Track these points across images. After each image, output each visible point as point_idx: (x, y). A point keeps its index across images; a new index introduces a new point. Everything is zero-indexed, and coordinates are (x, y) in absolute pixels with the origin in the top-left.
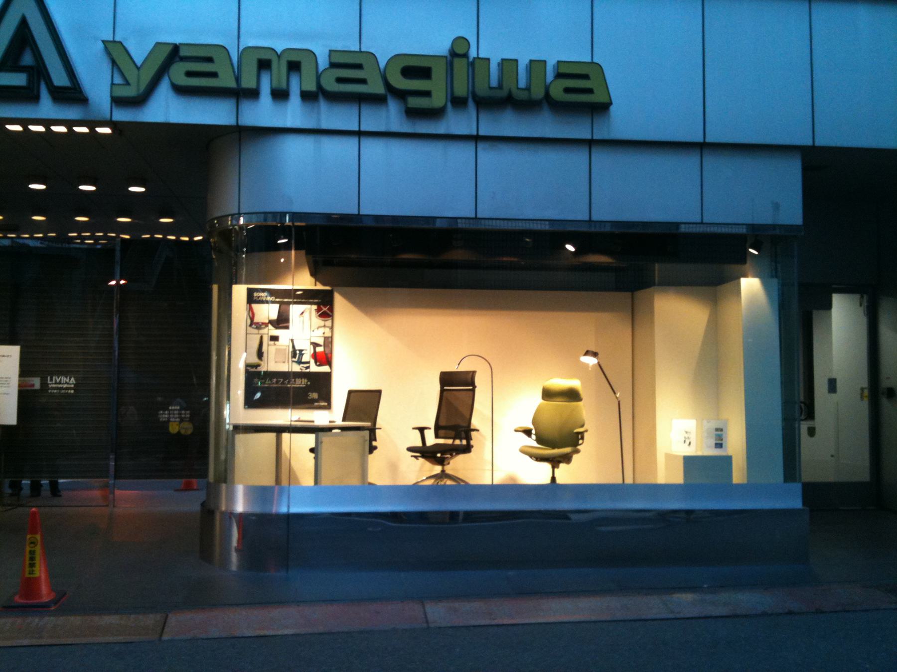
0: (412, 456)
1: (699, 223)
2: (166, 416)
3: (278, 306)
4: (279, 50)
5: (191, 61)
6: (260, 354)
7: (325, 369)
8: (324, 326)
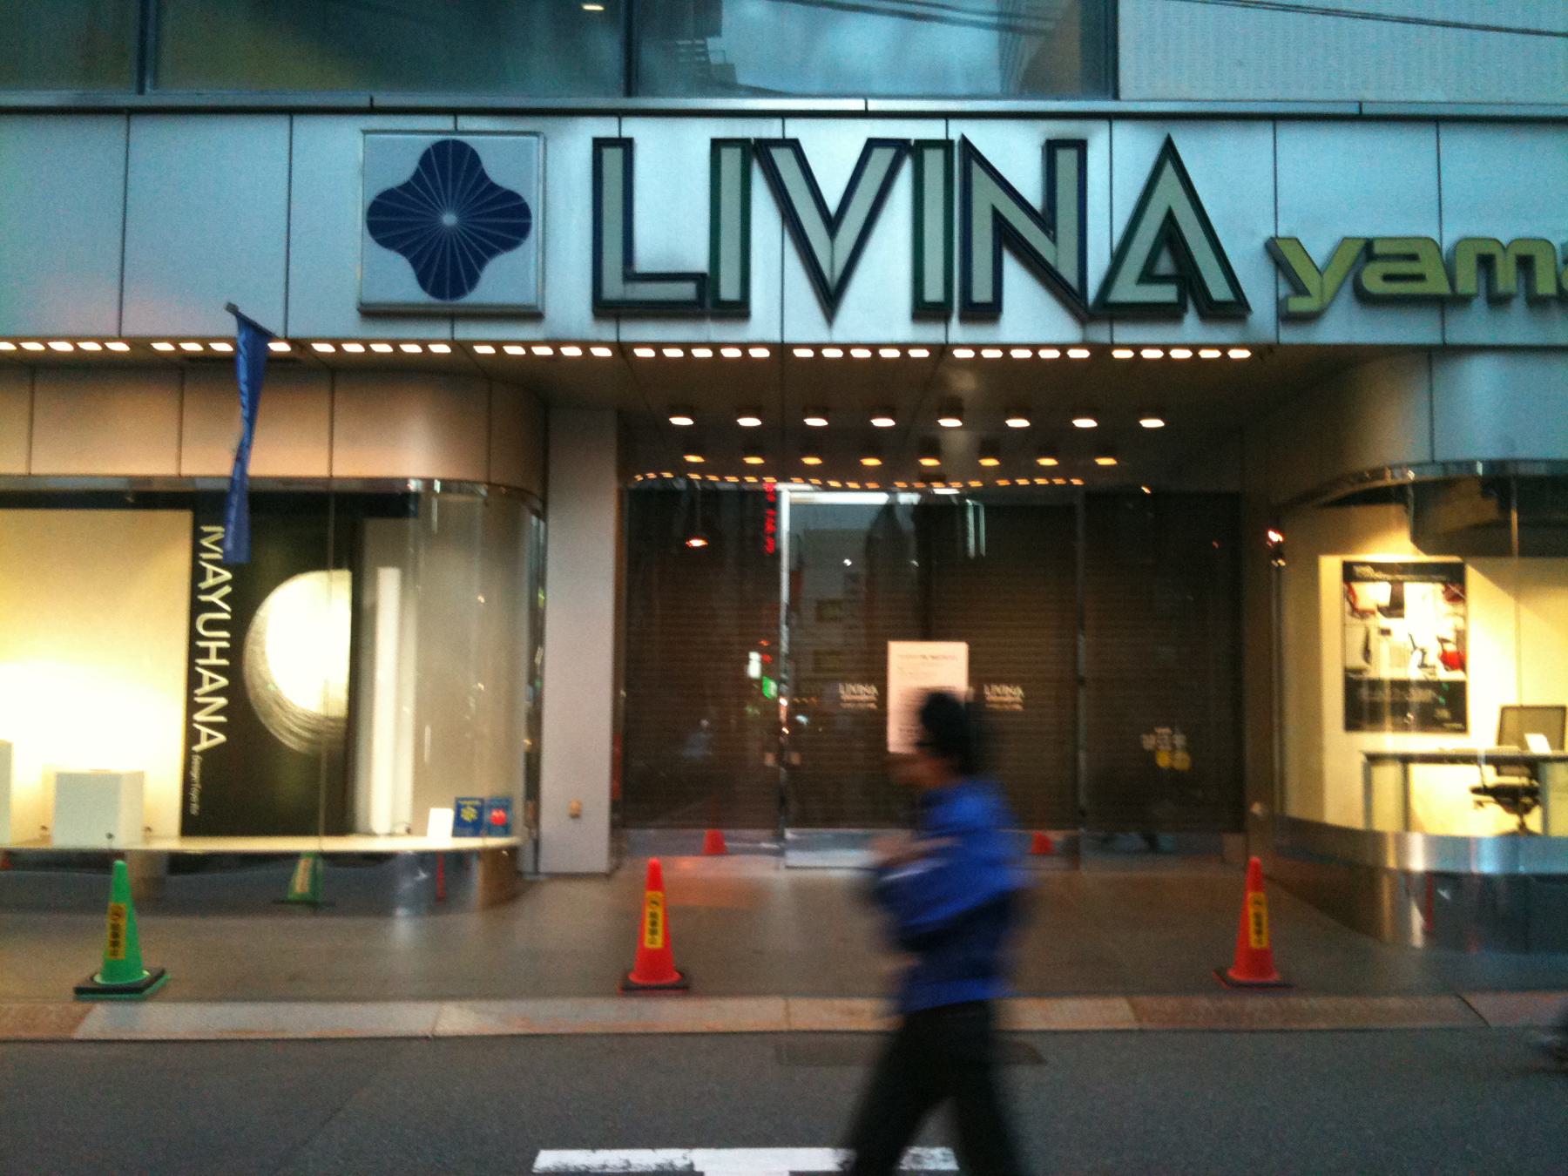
1: (1426, 464)
4: (1504, 241)
6: (1367, 653)
7: (1456, 675)
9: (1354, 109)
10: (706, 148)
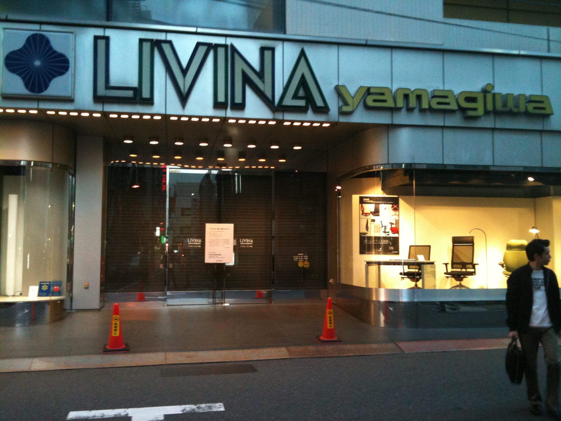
0: (446, 277)
2: (297, 258)
3: (374, 205)
5: (375, 95)
6: (367, 228)
7: (396, 235)
8: (395, 215)
9: (364, 42)
10: (137, 42)
